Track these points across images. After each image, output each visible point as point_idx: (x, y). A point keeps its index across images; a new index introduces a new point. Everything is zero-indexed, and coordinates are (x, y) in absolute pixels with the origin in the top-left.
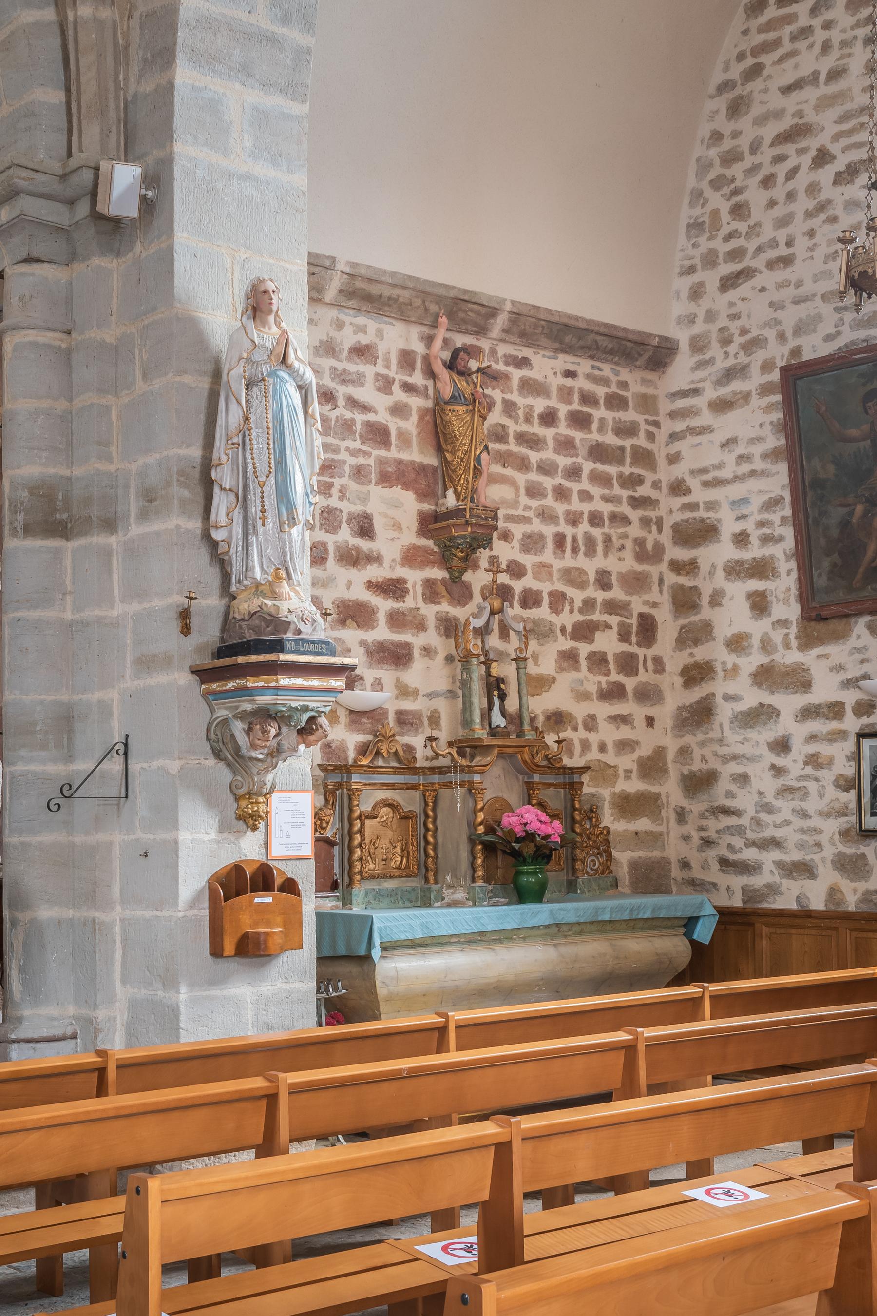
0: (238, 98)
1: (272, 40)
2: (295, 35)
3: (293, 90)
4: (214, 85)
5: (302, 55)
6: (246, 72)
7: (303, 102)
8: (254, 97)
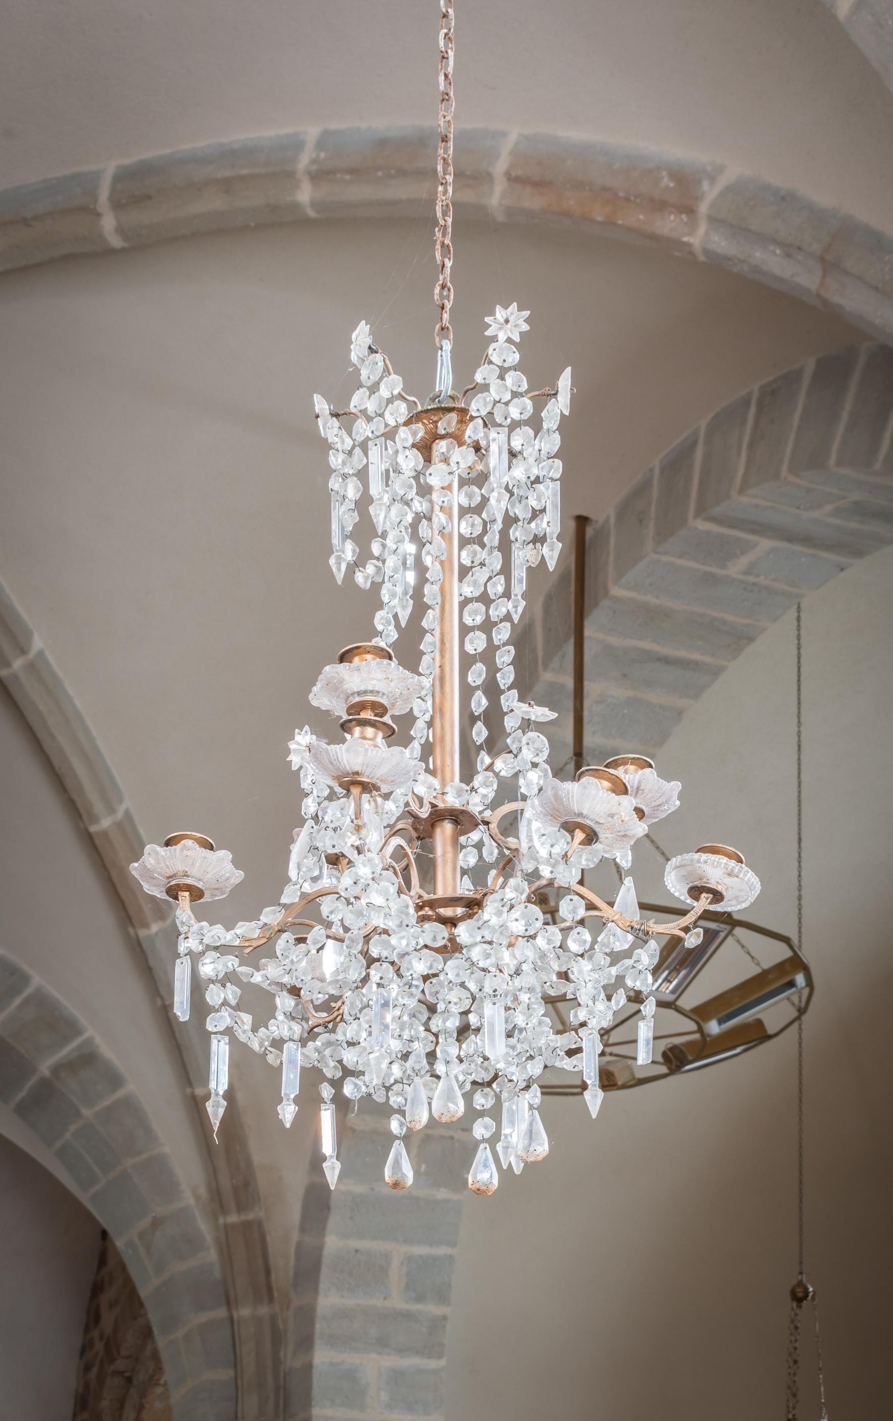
0: (373, 1366)
1: (408, 1316)
2: (432, 1309)
3: (431, 1349)
4: (349, 1359)
5: (437, 1324)
6: (382, 1344)
7: (440, 1356)
8: (390, 1361)
